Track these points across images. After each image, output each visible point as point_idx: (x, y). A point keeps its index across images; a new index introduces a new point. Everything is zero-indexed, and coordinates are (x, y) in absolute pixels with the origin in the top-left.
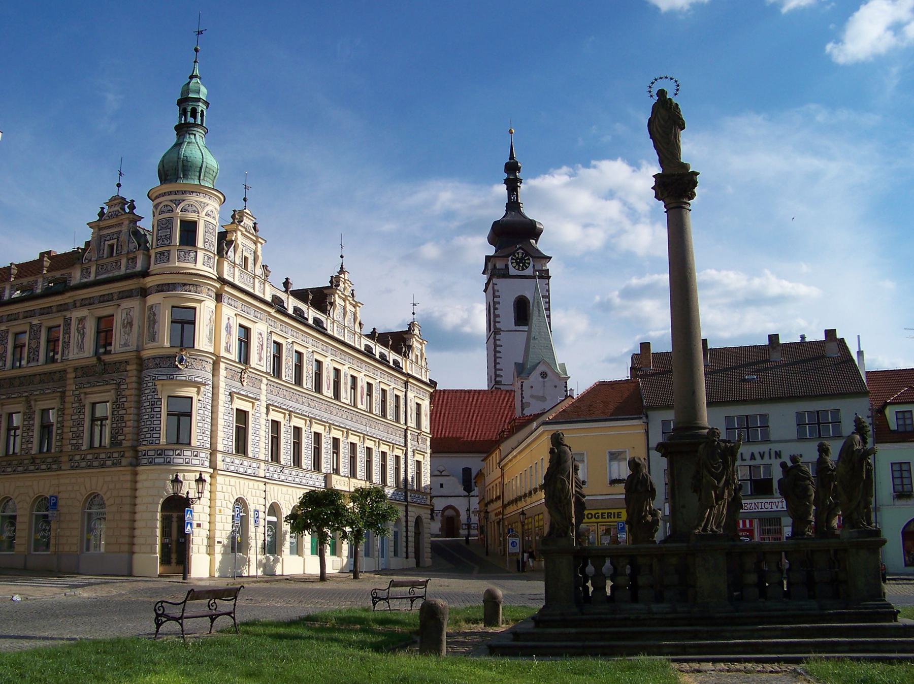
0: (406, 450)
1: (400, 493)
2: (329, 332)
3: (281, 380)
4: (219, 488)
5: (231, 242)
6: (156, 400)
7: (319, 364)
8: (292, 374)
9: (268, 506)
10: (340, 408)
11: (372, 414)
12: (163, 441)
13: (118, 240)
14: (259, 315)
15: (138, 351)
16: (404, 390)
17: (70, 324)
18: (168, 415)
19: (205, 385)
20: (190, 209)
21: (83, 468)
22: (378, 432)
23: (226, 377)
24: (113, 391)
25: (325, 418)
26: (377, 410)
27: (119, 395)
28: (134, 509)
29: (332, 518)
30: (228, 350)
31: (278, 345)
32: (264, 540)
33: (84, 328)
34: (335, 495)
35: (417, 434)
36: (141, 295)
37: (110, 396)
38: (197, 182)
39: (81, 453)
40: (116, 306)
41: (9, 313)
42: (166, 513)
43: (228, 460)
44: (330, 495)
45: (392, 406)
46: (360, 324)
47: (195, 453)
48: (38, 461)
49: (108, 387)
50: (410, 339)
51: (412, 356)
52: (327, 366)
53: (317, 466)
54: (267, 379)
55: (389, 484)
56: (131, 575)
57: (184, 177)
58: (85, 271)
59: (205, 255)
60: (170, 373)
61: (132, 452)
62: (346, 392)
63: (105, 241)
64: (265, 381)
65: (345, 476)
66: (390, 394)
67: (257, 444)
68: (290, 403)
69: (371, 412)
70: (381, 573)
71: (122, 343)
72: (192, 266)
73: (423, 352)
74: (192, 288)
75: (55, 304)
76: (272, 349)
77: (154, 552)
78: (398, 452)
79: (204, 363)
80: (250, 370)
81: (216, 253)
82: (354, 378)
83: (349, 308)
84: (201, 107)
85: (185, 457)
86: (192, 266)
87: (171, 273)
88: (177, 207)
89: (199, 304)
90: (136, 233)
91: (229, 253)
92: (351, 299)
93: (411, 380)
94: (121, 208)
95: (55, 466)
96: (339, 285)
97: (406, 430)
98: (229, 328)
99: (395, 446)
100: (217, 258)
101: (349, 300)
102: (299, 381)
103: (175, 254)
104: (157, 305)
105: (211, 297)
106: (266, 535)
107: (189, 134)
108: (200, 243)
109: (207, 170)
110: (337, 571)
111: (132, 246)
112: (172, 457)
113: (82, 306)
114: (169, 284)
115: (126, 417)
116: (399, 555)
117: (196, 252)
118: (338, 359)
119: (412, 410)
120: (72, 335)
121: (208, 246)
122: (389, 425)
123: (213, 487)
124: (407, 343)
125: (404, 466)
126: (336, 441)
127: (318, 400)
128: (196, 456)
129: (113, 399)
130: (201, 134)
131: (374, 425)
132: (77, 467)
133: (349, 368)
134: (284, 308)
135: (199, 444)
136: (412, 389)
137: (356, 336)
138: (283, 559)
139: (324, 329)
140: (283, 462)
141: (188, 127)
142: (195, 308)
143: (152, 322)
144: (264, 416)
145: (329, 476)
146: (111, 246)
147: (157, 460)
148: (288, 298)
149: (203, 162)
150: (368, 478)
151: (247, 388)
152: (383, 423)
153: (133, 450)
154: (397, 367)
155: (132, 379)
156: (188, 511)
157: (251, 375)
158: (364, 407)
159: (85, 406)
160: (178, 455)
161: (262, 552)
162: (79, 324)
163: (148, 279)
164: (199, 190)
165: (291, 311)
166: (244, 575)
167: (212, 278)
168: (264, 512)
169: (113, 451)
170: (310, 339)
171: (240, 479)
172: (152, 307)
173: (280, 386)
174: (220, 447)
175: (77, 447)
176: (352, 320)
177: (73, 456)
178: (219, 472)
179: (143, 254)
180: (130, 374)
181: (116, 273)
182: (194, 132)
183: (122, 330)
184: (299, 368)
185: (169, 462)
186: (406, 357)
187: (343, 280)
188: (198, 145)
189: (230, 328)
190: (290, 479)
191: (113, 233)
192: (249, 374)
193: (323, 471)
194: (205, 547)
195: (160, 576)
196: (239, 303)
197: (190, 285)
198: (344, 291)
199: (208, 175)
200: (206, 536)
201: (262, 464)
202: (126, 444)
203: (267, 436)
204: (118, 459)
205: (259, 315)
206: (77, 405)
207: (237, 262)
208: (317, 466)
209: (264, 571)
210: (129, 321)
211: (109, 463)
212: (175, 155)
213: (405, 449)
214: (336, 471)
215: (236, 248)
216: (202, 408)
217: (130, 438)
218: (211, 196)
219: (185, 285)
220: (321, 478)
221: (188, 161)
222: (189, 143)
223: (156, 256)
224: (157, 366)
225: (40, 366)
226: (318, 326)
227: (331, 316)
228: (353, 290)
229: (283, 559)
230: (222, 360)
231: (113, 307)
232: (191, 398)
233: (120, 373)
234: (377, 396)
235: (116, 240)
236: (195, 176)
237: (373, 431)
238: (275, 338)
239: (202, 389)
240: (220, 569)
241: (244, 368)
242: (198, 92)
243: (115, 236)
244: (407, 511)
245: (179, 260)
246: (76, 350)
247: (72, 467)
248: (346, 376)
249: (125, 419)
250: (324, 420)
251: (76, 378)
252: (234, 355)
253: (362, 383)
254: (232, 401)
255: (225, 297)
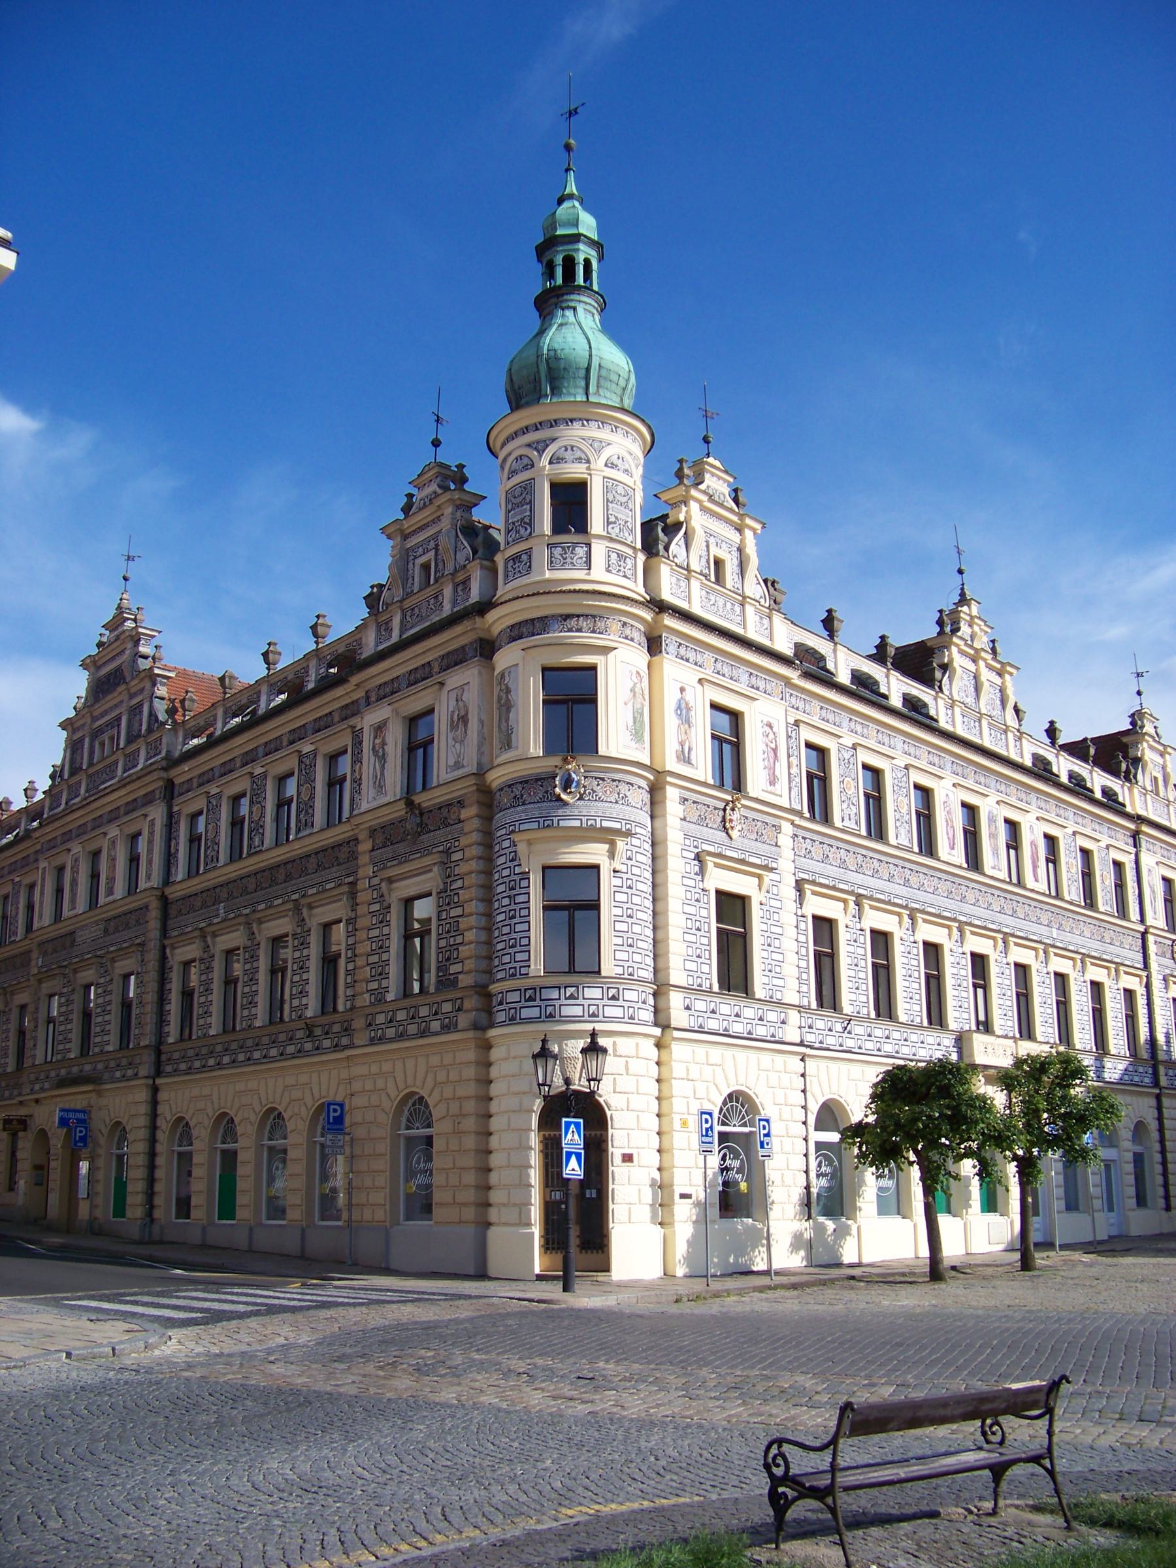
0: (1148, 977)
1: (1141, 1069)
2: (943, 724)
3: (833, 827)
4: (678, 1070)
5: (678, 526)
6: (517, 878)
7: (925, 793)
8: (858, 814)
9: (814, 1108)
10: (984, 889)
11: (1063, 900)
12: (537, 967)
13: (436, 554)
14: (761, 684)
15: (480, 774)
16: (1133, 850)
17: (361, 743)
18: (545, 908)
19: (628, 834)
20: (569, 455)
21: (391, 1040)
22: (1079, 940)
23: (684, 819)
24: (436, 869)
25: (949, 910)
26: (1073, 890)
27: (449, 876)
28: (487, 1125)
29: (945, 1128)
30: (685, 758)
31: (821, 753)
32: (808, 1188)
33: (384, 744)
34: (951, 1072)
35: (1170, 943)
36: (481, 655)
37: (431, 880)
38: (581, 398)
39: (385, 1008)
40: (437, 687)
41: (266, 740)
42: (552, 1133)
43: (700, 1005)
44: (940, 1073)
45: (1107, 883)
46: (1017, 710)
47: (612, 992)
48: (318, 1031)
49: (427, 861)
50: (1136, 744)
51: (1143, 779)
52: (944, 799)
53: (936, 1015)
54: (792, 823)
55: (1113, 1051)
56: (482, 1275)
57: (553, 394)
58: (383, 628)
59: (609, 550)
60: (544, 813)
61: (475, 997)
62: (996, 853)
63: (416, 557)
64: (787, 828)
65: (1006, 1037)
66: (1102, 859)
67: (778, 969)
68: (858, 878)
69: (1058, 896)
70: (1100, 1248)
71: (451, 762)
72: (580, 574)
73: (1169, 770)
74: (582, 623)
75: (336, 705)
76: (804, 762)
77: (524, 1221)
78: (1133, 983)
79: (623, 788)
80: (744, 802)
81: (639, 546)
82: (1013, 826)
83: (986, 675)
84: (584, 252)
85: (586, 1003)
86: (580, 574)
87: (534, 594)
88: (541, 456)
89: (602, 658)
90: (471, 531)
91: (673, 547)
92: (989, 657)
93: (1145, 828)
94: (439, 486)
95: (345, 1041)
96: (958, 629)
97: (1144, 935)
98: (683, 711)
99: (1122, 968)
100: (641, 557)
101: (985, 660)
102: (877, 828)
103: (542, 555)
104: (512, 669)
105: (632, 640)
106: (813, 1174)
107: (563, 309)
108: (596, 524)
109: (603, 373)
110: (1001, 1247)
111: (461, 558)
112: (557, 1003)
113: (379, 699)
114: (532, 620)
115: (464, 923)
116: (1149, 1203)
117: (589, 545)
118: (970, 783)
119: (1153, 892)
120: (365, 761)
121: (617, 530)
122: (1103, 924)
123: (663, 1069)
124: (1132, 753)
125: (1146, 1011)
126: (979, 963)
127: (930, 872)
128: (614, 998)
129: (438, 886)
130: (588, 307)
131: (1067, 924)
132: (380, 1039)
133: (998, 803)
134: (828, 671)
135: (620, 970)
136: (1151, 847)
137: (1010, 735)
138: (859, 1228)
139: (932, 718)
140: (847, 1009)
141: (558, 296)
142: (593, 668)
143: (504, 709)
144: (791, 906)
145: (965, 1036)
146: (426, 567)
147: (525, 1013)
148: (835, 651)
149: (590, 356)
150: (1064, 1039)
151: (741, 841)
152: (1089, 920)
153: (477, 993)
154: (1111, 801)
155: (470, 837)
156: (568, 1125)
157: (752, 815)
158: (1042, 886)
159: (389, 907)
160: (572, 997)
161: (801, 1213)
162: (375, 737)
163: (492, 616)
164: (586, 414)
165: (896, 701)
166: (755, 1269)
167: (628, 598)
168: (804, 1123)
169: (444, 998)
170: (898, 741)
171: (735, 1049)
172: (502, 675)
173: (830, 841)
174: (677, 977)
175: (379, 997)
176: (998, 703)
177: (373, 1015)
178: (676, 1034)
179: (482, 567)
180: (467, 827)
181: (435, 618)
182: (572, 304)
183: (450, 736)
184: (875, 801)
185: (551, 1016)
186: (1129, 781)
187: (968, 618)
188: (581, 328)
189: (688, 709)
190: (869, 1045)
191: (428, 540)
192: (744, 812)
193: (953, 1025)
194: (648, 1209)
195: (540, 1278)
196: (708, 658)
197: (578, 616)
198: (972, 640)
199: (608, 384)
200: (648, 1182)
201: (794, 1016)
202: (465, 980)
203: (803, 951)
204: (452, 1015)
205: (761, 684)
206: (376, 907)
207: (695, 566)
208: (936, 1015)
209: (809, 1258)
210: (463, 713)
211: (435, 1025)
212: (532, 351)
213: (1144, 974)
214: (985, 1026)
215: (690, 538)
216: (624, 889)
217: (472, 966)
218: (616, 425)
219: (567, 617)
220: (948, 1041)
221: (557, 359)
222: (561, 325)
223: (506, 567)
224: (518, 801)
225: (319, 836)
226: (915, 711)
227: (946, 692)
228: (993, 641)
229: (859, 1228)
230: (669, 779)
231: (430, 690)
232: (596, 868)
233: (448, 829)
234: (1070, 865)
235: (432, 553)
236: (576, 387)
237: (1068, 937)
238: (807, 734)
239: (621, 844)
240: (689, 1259)
241: (729, 798)
242: (575, 223)
243: (432, 544)
244: (1159, 1108)
245: (552, 566)
246: (372, 792)
247: (372, 1039)
248: (992, 820)
249: (462, 926)
250: (945, 914)
251: (373, 850)
252: (703, 767)
253: (1032, 835)
254: (702, 872)
255: (670, 644)
